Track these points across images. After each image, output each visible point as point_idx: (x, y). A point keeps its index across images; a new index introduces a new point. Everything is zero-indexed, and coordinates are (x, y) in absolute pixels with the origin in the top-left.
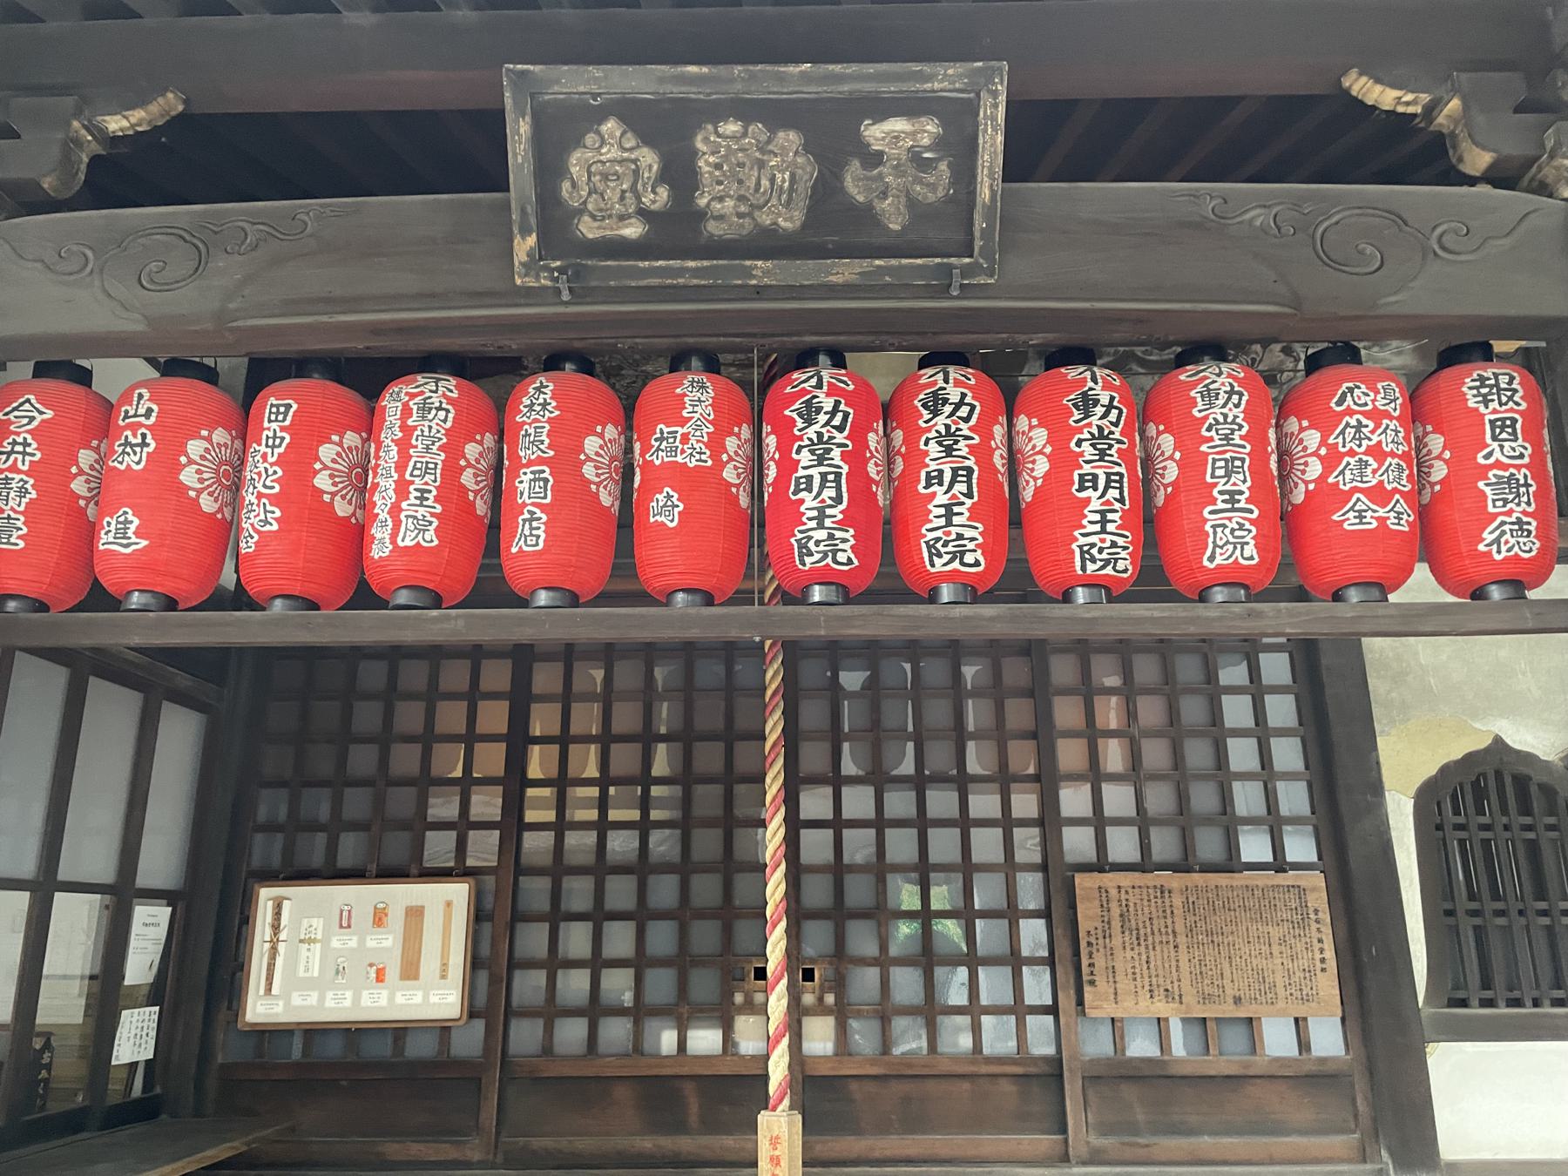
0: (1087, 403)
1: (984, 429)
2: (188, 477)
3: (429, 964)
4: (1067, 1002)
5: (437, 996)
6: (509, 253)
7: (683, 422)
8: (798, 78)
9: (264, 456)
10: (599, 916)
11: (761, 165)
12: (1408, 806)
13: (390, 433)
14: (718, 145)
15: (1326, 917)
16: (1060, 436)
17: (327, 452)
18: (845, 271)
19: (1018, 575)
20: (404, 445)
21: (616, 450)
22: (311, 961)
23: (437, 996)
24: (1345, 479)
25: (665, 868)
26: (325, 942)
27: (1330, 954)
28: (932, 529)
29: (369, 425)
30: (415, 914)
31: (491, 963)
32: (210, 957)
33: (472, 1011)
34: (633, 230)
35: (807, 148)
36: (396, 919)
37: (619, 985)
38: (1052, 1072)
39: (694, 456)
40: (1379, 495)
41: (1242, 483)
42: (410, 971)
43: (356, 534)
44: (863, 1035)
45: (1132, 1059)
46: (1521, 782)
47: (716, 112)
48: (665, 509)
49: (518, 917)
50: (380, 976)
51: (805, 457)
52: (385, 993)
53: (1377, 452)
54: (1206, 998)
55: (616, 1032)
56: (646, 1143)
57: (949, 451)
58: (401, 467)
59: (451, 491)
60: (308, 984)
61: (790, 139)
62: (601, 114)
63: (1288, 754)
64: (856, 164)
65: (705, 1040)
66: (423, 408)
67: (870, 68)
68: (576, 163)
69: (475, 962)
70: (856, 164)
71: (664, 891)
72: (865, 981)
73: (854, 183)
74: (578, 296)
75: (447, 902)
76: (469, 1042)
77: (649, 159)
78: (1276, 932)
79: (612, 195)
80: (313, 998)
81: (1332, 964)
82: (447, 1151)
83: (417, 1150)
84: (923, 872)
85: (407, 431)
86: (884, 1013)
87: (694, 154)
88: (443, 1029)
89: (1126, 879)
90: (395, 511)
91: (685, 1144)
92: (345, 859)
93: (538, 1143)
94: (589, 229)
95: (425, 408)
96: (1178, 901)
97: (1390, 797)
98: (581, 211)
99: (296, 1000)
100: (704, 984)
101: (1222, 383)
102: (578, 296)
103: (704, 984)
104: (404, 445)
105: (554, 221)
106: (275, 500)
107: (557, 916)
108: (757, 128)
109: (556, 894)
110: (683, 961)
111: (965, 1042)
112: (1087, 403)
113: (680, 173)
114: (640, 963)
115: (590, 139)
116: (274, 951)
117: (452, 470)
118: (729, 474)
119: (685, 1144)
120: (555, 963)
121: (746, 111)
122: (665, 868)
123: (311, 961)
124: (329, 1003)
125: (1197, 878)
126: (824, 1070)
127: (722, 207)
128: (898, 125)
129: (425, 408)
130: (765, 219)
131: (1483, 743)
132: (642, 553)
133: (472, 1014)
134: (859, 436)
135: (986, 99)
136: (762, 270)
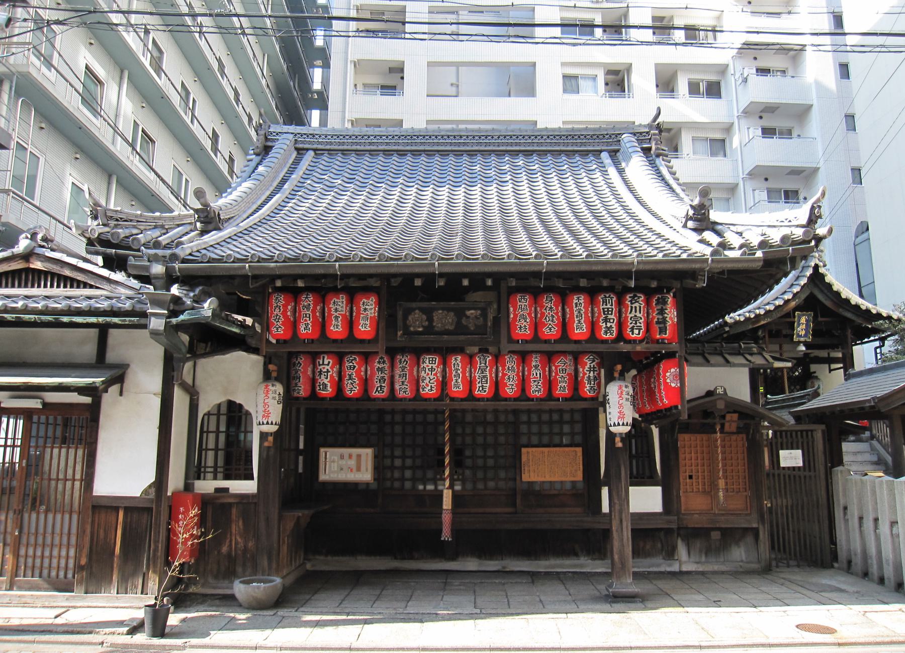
3: (363, 468)
5: (366, 475)
6: (397, 334)
14: (438, 315)
22: (335, 467)
23: (366, 475)
30: (359, 456)
31: (378, 468)
32: (313, 464)
34: (420, 329)
36: (354, 457)
42: (359, 469)
45: (325, 484)
49: (384, 457)
50: (351, 470)
60: (334, 472)
61: (452, 314)
62: (414, 309)
65: (430, 487)
68: (410, 318)
73: (464, 321)
77: (424, 317)
80: (336, 475)
84: (485, 446)
88: (368, 484)
105: (406, 328)
113: (430, 319)
121: (443, 309)
127: (438, 325)
128: (472, 311)
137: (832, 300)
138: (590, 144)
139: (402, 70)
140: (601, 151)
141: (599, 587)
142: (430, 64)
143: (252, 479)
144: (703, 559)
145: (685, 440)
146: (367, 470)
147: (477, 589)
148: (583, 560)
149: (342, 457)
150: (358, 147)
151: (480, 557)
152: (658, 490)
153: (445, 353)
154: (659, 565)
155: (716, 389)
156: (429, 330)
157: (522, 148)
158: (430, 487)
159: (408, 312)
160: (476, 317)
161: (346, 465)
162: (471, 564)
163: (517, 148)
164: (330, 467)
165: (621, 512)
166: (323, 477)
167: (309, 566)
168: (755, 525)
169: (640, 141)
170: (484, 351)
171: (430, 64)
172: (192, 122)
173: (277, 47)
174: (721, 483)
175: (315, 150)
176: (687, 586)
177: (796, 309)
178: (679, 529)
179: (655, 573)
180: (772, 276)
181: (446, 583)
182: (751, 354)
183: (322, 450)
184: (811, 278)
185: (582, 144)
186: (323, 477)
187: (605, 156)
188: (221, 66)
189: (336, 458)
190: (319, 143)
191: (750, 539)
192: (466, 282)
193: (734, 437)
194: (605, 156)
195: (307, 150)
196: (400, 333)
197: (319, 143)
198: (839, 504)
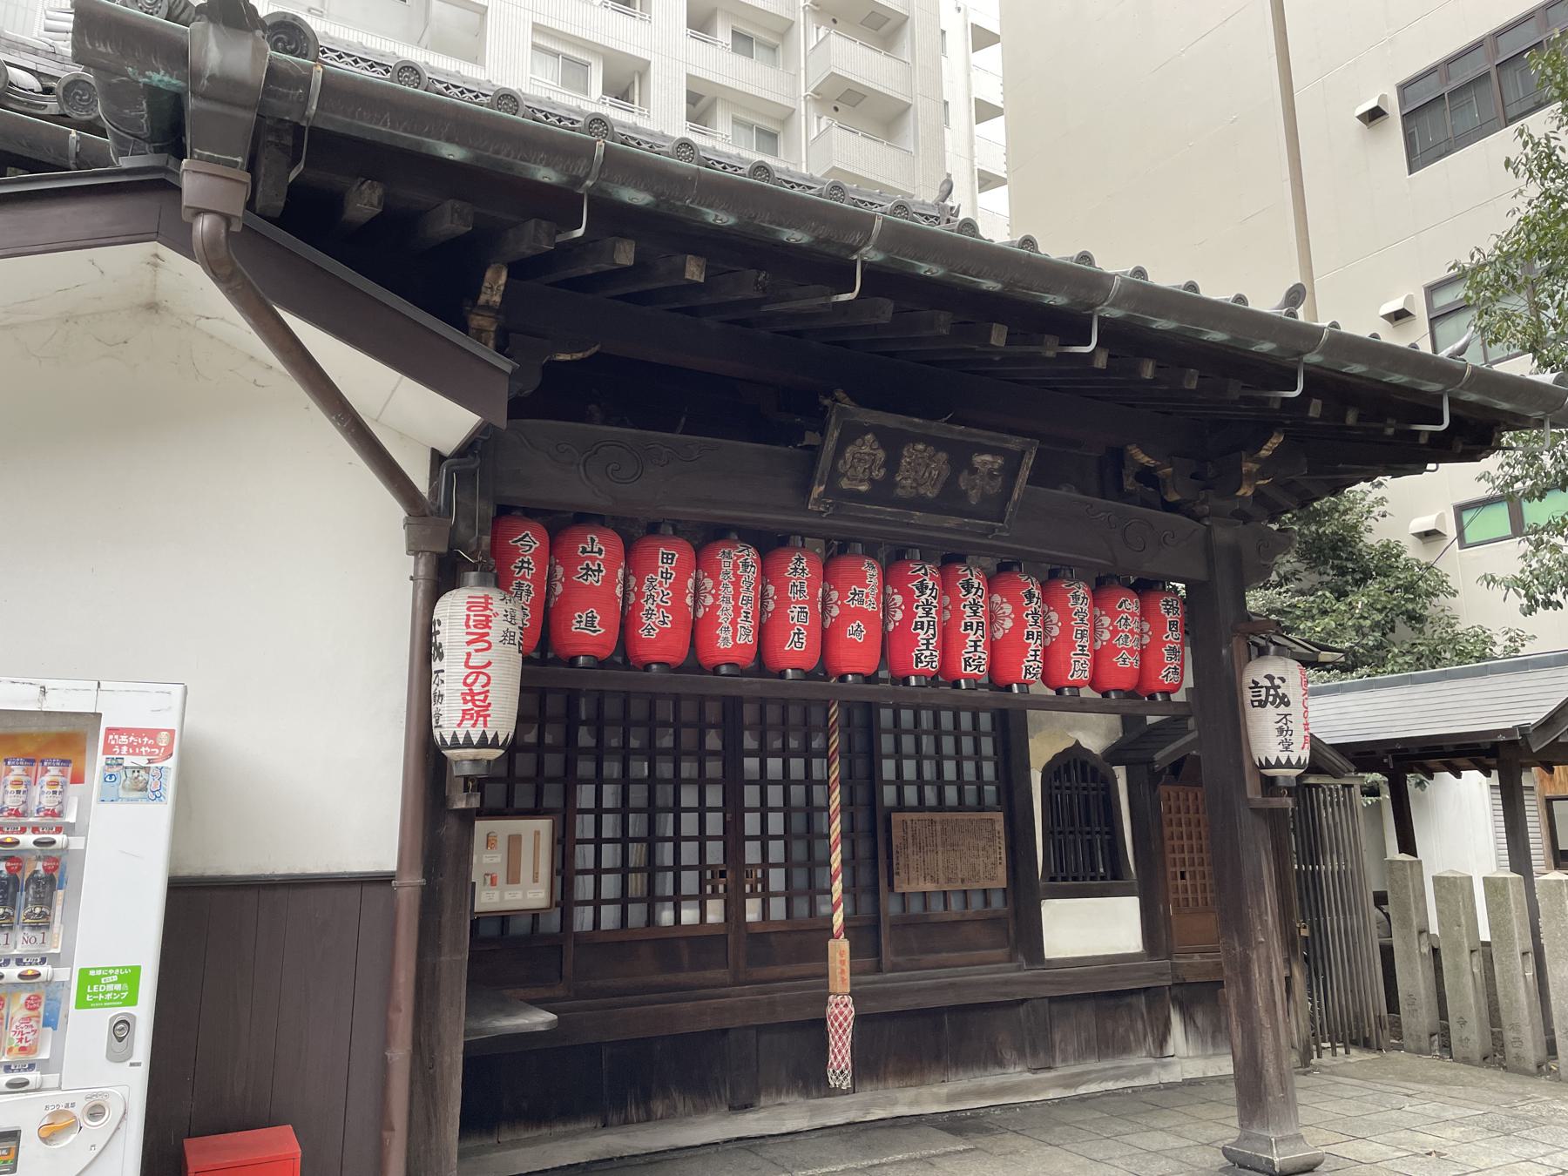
7: (866, 586)
9: (661, 584)
11: (928, 466)
15: (1002, 834)
16: (1018, 610)
18: (952, 522)
20: (736, 585)
27: (1003, 855)
30: (514, 841)
33: (553, 903)
34: (863, 488)
35: (949, 461)
36: (502, 843)
42: (513, 877)
46: (1084, 764)
47: (916, 439)
50: (493, 883)
52: (497, 893)
54: (949, 880)
57: (975, 613)
61: (943, 456)
62: (866, 431)
63: (987, 746)
64: (966, 472)
67: (987, 433)
68: (849, 451)
70: (966, 472)
76: (553, 923)
77: (881, 455)
78: (981, 844)
79: (860, 469)
85: (738, 577)
87: (902, 456)
88: (535, 915)
89: (915, 816)
90: (734, 623)
91: (683, 977)
94: (845, 484)
96: (939, 827)
97: (1033, 772)
98: (844, 475)
104: (736, 585)
108: (931, 449)
113: (892, 464)
115: (859, 441)
119: (683, 977)
124: (530, 896)
125: (948, 815)
126: (758, 930)
128: (988, 458)
129: (745, 565)
130: (922, 491)
131: (1070, 744)
135: (1027, 455)
136: (918, 516)
143: (1437, 880)
144: (1210, 1052)
146: (535, 880)
148: (1016, 1074)
152: (1129, 907)
154: (1145, 1071)
156: (883, 491)
159: (851, 434)
160: (990, 472)
196: (818, 490)
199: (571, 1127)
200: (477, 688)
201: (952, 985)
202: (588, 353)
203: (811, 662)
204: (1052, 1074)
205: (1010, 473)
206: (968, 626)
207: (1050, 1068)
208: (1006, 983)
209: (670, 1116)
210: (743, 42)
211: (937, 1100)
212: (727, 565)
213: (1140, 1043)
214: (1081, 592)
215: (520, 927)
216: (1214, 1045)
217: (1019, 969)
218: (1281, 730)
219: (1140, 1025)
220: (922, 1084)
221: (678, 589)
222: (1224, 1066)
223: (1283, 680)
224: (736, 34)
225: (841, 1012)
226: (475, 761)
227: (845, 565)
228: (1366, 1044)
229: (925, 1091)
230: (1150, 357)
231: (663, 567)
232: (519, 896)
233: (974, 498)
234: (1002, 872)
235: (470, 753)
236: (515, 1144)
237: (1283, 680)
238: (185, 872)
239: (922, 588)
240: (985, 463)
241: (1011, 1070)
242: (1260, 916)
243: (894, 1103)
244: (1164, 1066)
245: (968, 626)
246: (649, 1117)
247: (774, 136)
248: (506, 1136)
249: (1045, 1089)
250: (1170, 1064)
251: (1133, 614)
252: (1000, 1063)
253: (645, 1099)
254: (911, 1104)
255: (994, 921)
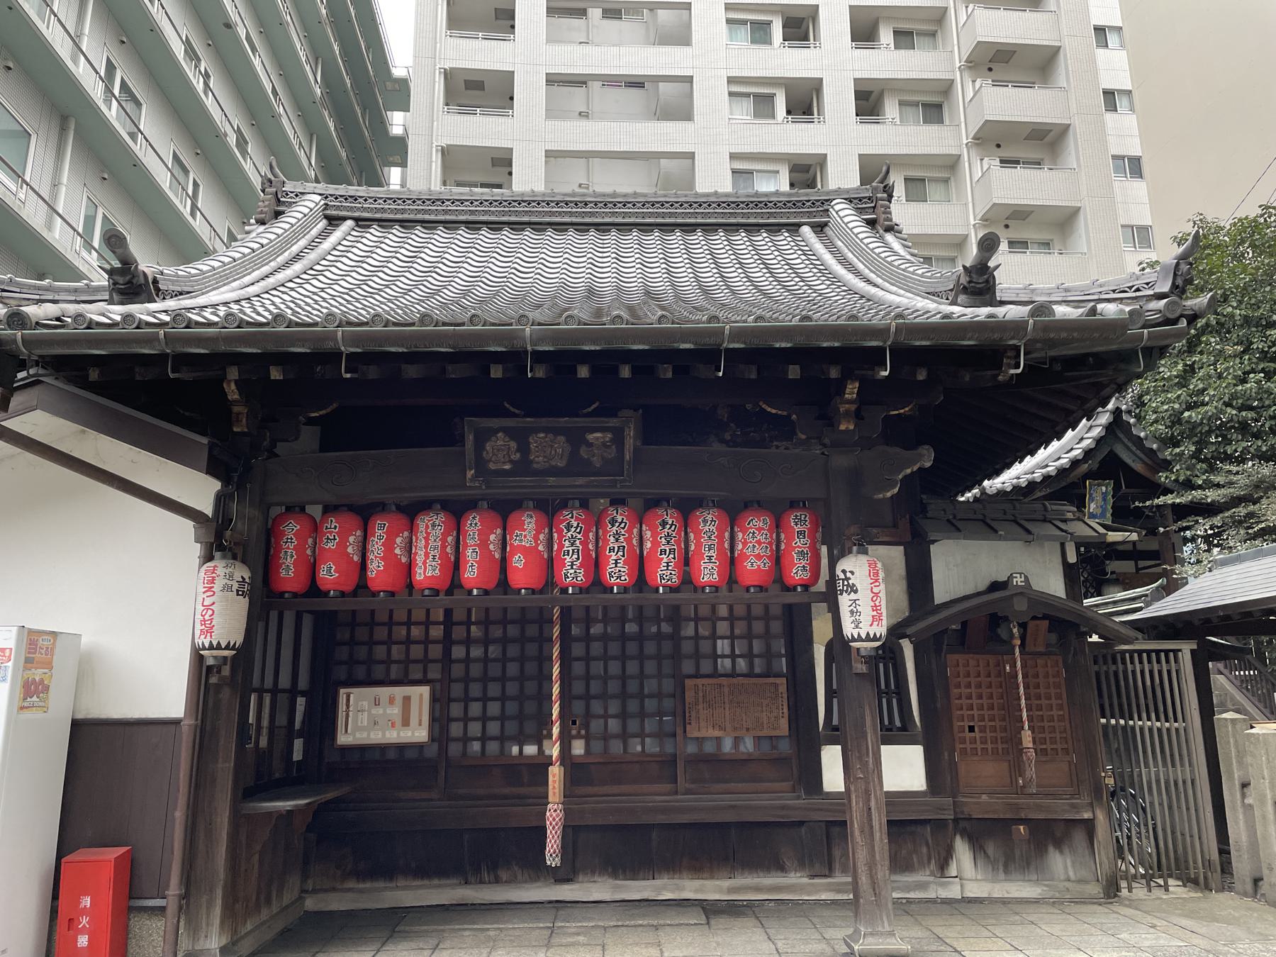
0: (664, 524)
1: (630, 531)
2: (350, 550)
4: (679, 731)
8: (564, 421)
10: (485, 699)
12: (823, 649)
13: (421, 535)
14: (535, 441)
15: (785, 696)
17: (399, 540)
18: (581, 481)
19: (641, 581)
20: (427, 539)
21: (500, 537)
22: (364, 719)
24: (748, 552)
25: (514, 641)
26: (369, 711)
27: (786, 710)
28: (610, 568)
29: (412, 528)
30: (407, 700)
31: (439, 720)
32: (324, 717)
33: (432, 738)
34: (507, 467)
35: (567, 441)
36: (399, 701)
37: (493, 728)
38: (672, 761)
39: (527, 542)
40: (759, 557)
41: (713, 553)
42: (406, 722)
43: (410, 567)
44: (597, 746)
47: (536, 430)
48: (518, 561)
50: (393, 725)
51: (567, 544)
53: (759, 542)
55: (493, 747)
56: (507, 791)
57: (617, 540)
58: (426, 547)
59: (443, 554)
60: (362, 729)
61: (562, 439)
62: (496, 431)
65: (530, 750)
66: (432, 528)
69: (433, 719)
71: (512, 689)
72: (596, 726)
73: (583, 452)
74: (487, 487)
75: (422, 693)
76: (432, 752)
77: (513, 445)
80: (365, 735)
81: (786, 715)
82: (424, 795)
83: (412, 795)
85: (428, 534)
86: (606, 737)
88: (420, 747)
89: (724, 681)
90: (425, 563)
92: (393, 676)
93: (461, 791)
94: (492, 466)
95: (434, 525)
96: (726, 690)
98: (490, 461)
99: (358, 735)
100: (530, 727)
101: (709, 517)
102: (487, 487)
103: (530, 727)
104: (427, 539)
105: (480, 464)
106: (382, 559)
107: (467, 700)
108: (551, 436)
109: (466, 690)
110: (520, 717)
111: (639, 748)
112: (664, 524)
113: (524, 448)
114: (502, 718)
116: (347, 716)
117: (444, 547)
118: (541, 548)
120: (466, 719)
121: (547, 430)
122: (514, 641)
123: (364, 719)
124: (388, 735)
128: (599, 435)
129: (434, 525)
130: (553, 463)
132: (510, 576)
133: (433, 740)
134: (586, 536)
135: (627, 430)
137: (1144, 463)
138: (781, 215)
139: (509, 163)
140: (799, 225)
141: (830, 933)
142: (549, 154)
145: (959, 664)
147: (609, 940)
148: (796, 878)
149: (377, 703)
150: (427, 217)
151: (615, 875)
153: (549, 509)
154: (923, 886)
155: (1011, 577)
156: (523, 467)
157: (680, 221)
158: (530, 750)
159: (482, 437)
160: (604, 444)
161: (382, 717)
162: (599, 889)
163: (672, 220)
164: (356, 721)
165: (867, 793)
166: (343, 739)
167: (310, 904)
168: (1087, 815)
169: (860, 211)
170: (617, 502)
171: (549, 154)
172: (193, 214)
173: (331, 125)
174: (1027, 738)
175: (357, 220)
176: (986, 933)
177: (1089, 475)
178: (956, 820)
179: (920, 901)
180: (1069, 413)
181: (552, 929)
182: (1065, 521)
183: (342, 691)
184: (1109, 428)
185: (771, 215)
186: (343, 739)
187: (806, 230)
188: (242, 143)
189: (365, 704)
190: (365, 209)
191: (1079, 837)
192: (583, 372)
193: (1040, 661)
194: (806, 230)
195: (345, 219)
196: (470, 474)
197: (365, 209)
198: (1231, 777)
199: (443, 882)
200: (207, 617)
201: (733, 807)
202: (329, 410)
203: (536, 583)
204: (829, 880)
205: (619, 440)
206: (612, 550)
207: (825, 876)
208: (783, 807)
209: (512, 881)
210: (904, 38)
211: (720, 891)
212: (422, 527)
213: (922, 865)
214: (709, 517)
215: (410, 755)
216: (1006, 871)
217: (798, 798)
218: (852, 612)
219: (925, 850)
220: (712, 878)
221: (389, 546)
222: (850, 879)
223: (852, 573)
224: (897, 33)
225: (554, 816)
226: (215, 657)
227: (513, 518)
228: (1191, 881)
229: (709, 883)
230: (625, 363)
231: (379, 532)
232: (410, 734)
233: (597, 462)
234: (784, 723)
235: (215, 653)
236: (405, 888)
237: (852, 573)
238: (79, 716)
239: (569, 527)
240: (597, 438)
241: (792, 874)
242: (860, 758)
243: (682, 889)
244: (943, 885)
245: (612, 550)
246: (497, 881)
247: (939, 107)
248: (401, 882)
249: (817, 892)
250: (949, 883)
251: (760, 529)
252: (782, 868)
253: (494, 867)
254: (696, 891)
255: (779, 761)
